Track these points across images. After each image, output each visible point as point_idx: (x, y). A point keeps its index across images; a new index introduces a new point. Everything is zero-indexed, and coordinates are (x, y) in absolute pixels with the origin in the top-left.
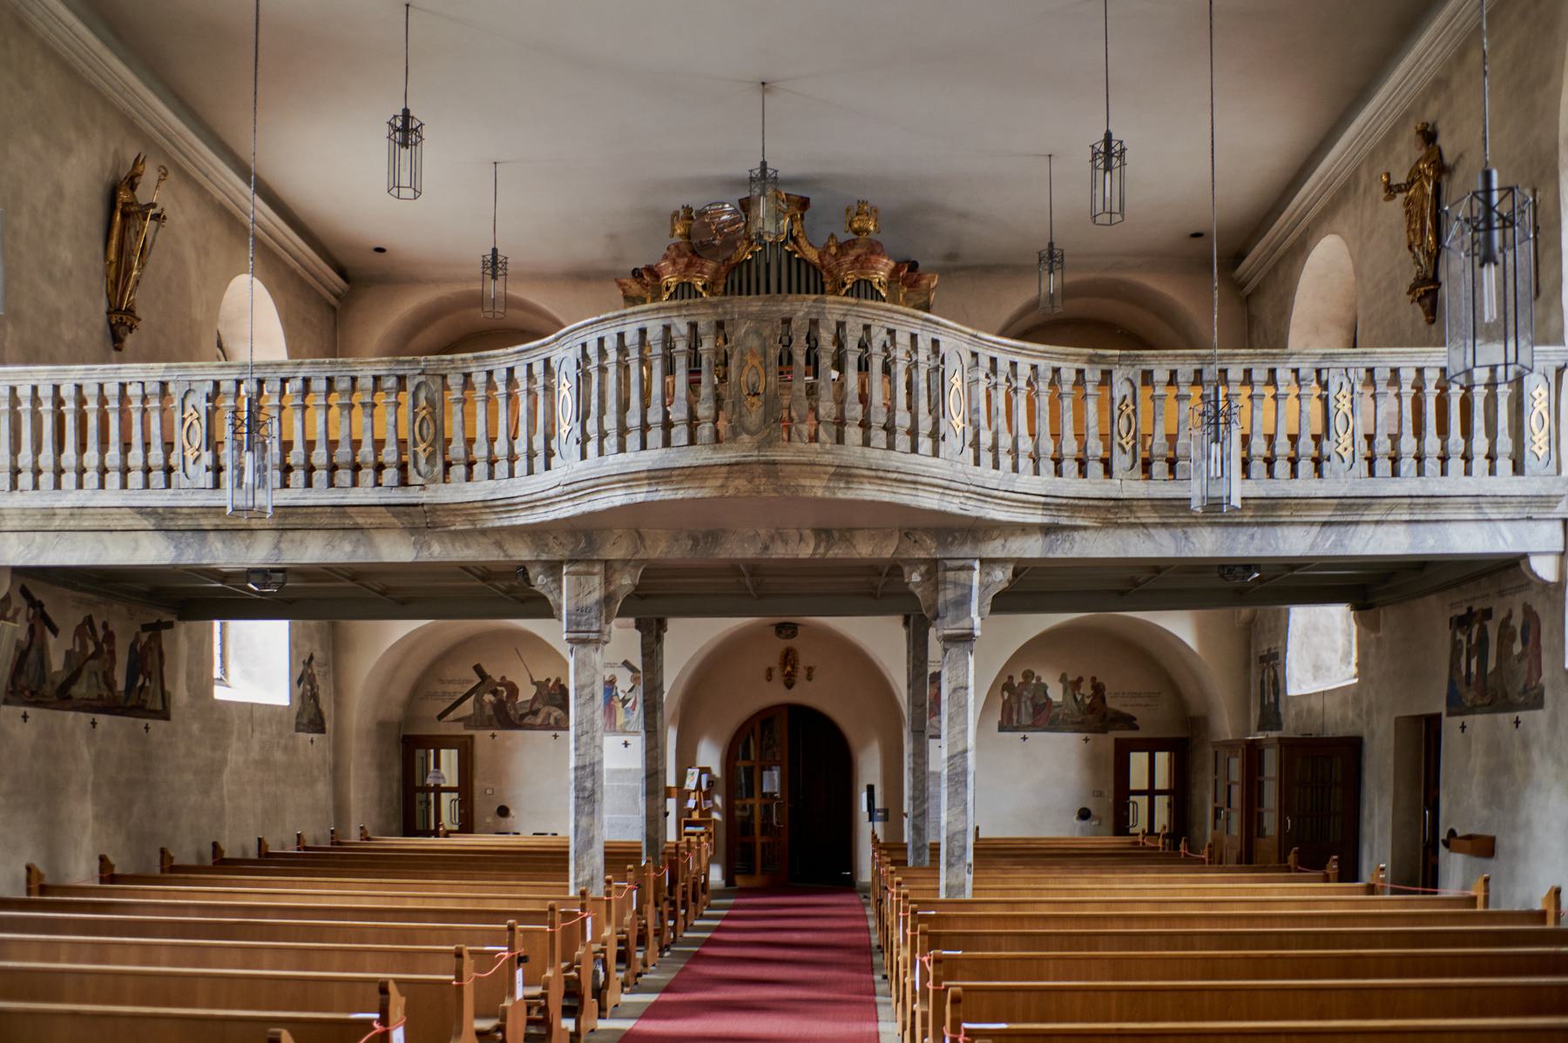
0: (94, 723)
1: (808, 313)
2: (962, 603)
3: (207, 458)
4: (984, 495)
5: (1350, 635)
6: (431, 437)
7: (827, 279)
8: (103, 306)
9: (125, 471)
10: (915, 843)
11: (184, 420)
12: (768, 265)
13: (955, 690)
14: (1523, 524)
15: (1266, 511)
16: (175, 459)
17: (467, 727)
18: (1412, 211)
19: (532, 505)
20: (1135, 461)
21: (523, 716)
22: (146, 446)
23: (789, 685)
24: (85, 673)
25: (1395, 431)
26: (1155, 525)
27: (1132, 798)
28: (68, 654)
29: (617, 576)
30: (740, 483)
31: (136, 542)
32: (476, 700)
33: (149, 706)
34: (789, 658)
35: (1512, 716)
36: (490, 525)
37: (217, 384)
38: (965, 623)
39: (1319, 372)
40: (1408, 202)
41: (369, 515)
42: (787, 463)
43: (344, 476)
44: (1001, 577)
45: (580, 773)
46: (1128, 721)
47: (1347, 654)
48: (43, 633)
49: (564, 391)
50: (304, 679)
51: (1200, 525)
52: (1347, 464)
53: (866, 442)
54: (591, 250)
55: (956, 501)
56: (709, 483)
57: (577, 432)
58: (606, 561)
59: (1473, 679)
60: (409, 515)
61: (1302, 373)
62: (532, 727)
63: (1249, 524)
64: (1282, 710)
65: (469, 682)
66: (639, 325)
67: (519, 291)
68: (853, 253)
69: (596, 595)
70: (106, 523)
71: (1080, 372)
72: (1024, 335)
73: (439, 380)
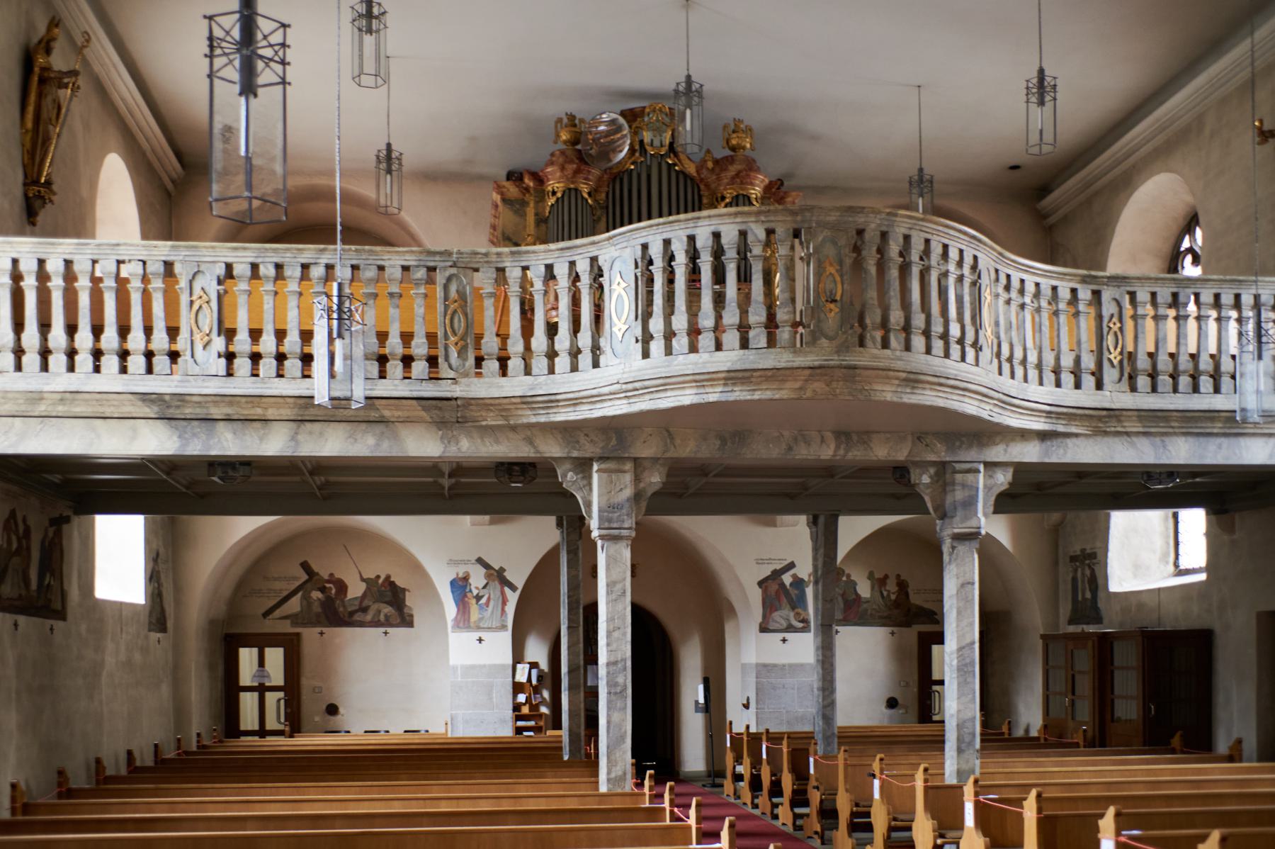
0: (16, 625)
1: (879, 225)
2: (970, 503)
4: (1007, 402)
5: (1168, 537)
6: (461, 332)
7: (705, 193)
8: (20, 177)
9: (124, 355)
10: (824, 731)
11: (192, 302)
13: (963, 585)
17: (295, 624)
19: (576, 402)
20: (1122, 375)
21: (352, 614)
22: (148, 331)
26: (1138, 434)
29: (646, 474)
30: (819, 386)
31: (135, 430)
32: (304, 597)
36: (525, 421)
37: (229, 267)
38: (973, 523)
41: (397, 408)
42: (866, 368)
44: (1003, 479)
45: (612, 668)
47: (1166, 555)
51: (1175, 434)
53: (928, 351)
55: (988, 407)
56: (788, 385)
57: (638, 331)
58: (635, 460)
60: (440, 409)
62: (362, 624)
63: (1217, 435)
65: (295, 578)
66: (712, 228)
68: (733, 170)
69: (628, 492)
70: (101, 409)
71: (1074, 291)
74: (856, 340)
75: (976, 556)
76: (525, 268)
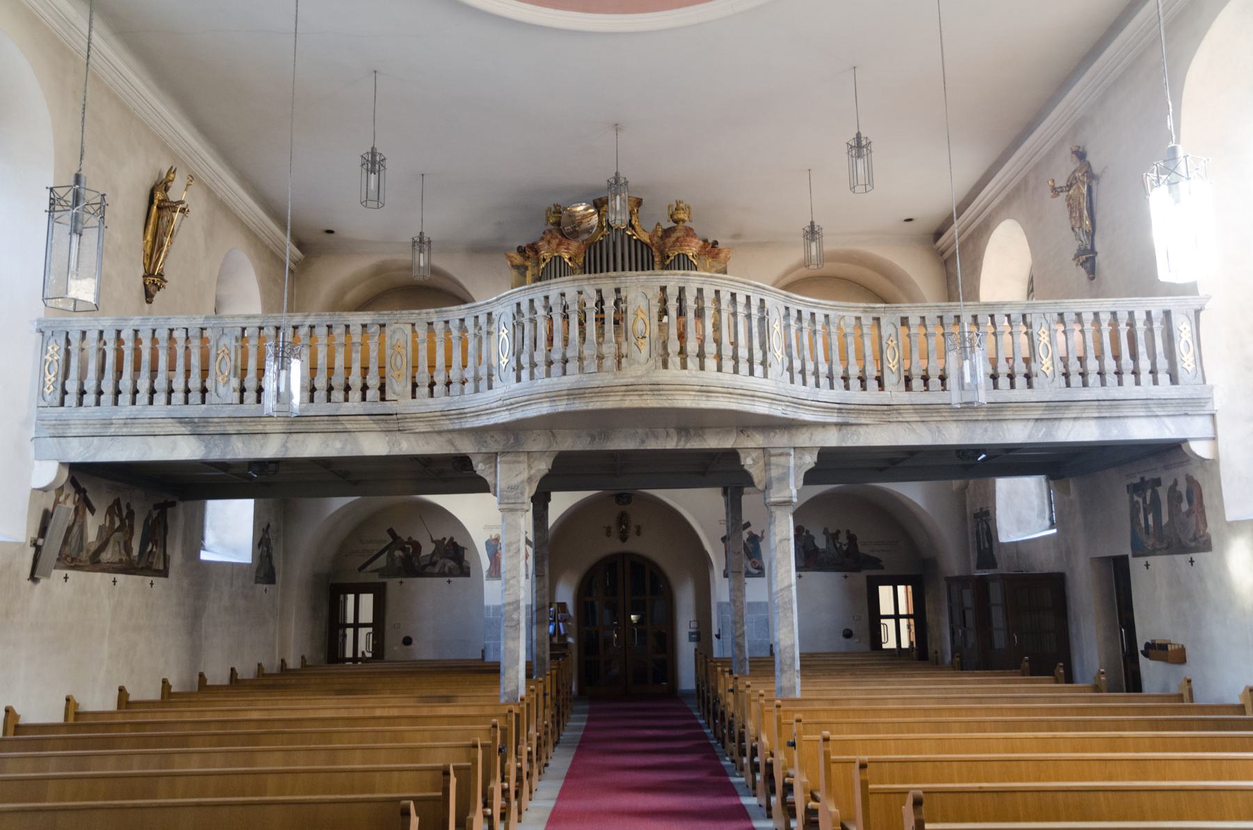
3: (235, 383)
11: (218, 355)
12: (614, 244)
14: (1182, 419)
15: (996, 411)
16: (209, 384)
17: (382, 576)
18: (1072, 206)
19: (477, 414)
21: (426, 566)
22: (188, 372)
23: (624, 539)
24: (111, 542)
25: (1081, 354)
27: (883, 621)
28: (101, 528)
33: (155, 567)
34: (623, 519)
35: (1187, 557)
39: (1024, 316)
40: (1069, 198)
43: (338, 395)
44: (810, 460)
46: (875, 563)
47: (1042, 511)
48: (84, 513)
49: (503, 335)
50: (263, 541)
52: (1050, 378)
54: (484, 231)
57: (514, 364)
59: (1151, 530)
61: (1012, 317)
62: (432, 575)
64: (995, 552)
67: (441, 263)
72: (787, 287)
73: (409, 327)
74: (660, 364)
75: (791, 518)
76: (447, 322)
